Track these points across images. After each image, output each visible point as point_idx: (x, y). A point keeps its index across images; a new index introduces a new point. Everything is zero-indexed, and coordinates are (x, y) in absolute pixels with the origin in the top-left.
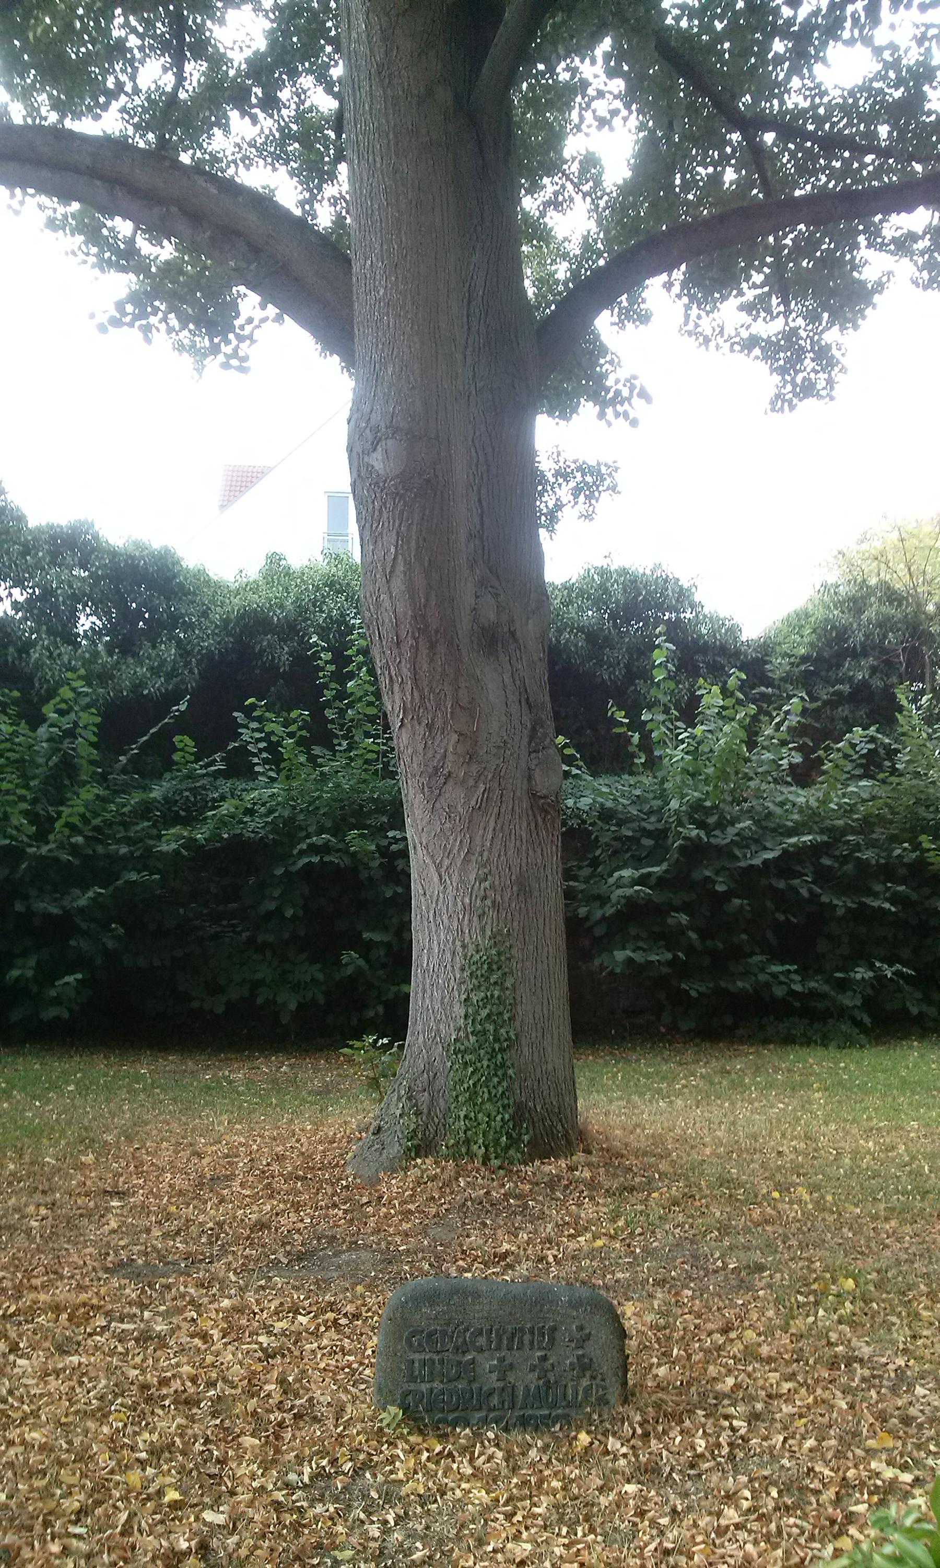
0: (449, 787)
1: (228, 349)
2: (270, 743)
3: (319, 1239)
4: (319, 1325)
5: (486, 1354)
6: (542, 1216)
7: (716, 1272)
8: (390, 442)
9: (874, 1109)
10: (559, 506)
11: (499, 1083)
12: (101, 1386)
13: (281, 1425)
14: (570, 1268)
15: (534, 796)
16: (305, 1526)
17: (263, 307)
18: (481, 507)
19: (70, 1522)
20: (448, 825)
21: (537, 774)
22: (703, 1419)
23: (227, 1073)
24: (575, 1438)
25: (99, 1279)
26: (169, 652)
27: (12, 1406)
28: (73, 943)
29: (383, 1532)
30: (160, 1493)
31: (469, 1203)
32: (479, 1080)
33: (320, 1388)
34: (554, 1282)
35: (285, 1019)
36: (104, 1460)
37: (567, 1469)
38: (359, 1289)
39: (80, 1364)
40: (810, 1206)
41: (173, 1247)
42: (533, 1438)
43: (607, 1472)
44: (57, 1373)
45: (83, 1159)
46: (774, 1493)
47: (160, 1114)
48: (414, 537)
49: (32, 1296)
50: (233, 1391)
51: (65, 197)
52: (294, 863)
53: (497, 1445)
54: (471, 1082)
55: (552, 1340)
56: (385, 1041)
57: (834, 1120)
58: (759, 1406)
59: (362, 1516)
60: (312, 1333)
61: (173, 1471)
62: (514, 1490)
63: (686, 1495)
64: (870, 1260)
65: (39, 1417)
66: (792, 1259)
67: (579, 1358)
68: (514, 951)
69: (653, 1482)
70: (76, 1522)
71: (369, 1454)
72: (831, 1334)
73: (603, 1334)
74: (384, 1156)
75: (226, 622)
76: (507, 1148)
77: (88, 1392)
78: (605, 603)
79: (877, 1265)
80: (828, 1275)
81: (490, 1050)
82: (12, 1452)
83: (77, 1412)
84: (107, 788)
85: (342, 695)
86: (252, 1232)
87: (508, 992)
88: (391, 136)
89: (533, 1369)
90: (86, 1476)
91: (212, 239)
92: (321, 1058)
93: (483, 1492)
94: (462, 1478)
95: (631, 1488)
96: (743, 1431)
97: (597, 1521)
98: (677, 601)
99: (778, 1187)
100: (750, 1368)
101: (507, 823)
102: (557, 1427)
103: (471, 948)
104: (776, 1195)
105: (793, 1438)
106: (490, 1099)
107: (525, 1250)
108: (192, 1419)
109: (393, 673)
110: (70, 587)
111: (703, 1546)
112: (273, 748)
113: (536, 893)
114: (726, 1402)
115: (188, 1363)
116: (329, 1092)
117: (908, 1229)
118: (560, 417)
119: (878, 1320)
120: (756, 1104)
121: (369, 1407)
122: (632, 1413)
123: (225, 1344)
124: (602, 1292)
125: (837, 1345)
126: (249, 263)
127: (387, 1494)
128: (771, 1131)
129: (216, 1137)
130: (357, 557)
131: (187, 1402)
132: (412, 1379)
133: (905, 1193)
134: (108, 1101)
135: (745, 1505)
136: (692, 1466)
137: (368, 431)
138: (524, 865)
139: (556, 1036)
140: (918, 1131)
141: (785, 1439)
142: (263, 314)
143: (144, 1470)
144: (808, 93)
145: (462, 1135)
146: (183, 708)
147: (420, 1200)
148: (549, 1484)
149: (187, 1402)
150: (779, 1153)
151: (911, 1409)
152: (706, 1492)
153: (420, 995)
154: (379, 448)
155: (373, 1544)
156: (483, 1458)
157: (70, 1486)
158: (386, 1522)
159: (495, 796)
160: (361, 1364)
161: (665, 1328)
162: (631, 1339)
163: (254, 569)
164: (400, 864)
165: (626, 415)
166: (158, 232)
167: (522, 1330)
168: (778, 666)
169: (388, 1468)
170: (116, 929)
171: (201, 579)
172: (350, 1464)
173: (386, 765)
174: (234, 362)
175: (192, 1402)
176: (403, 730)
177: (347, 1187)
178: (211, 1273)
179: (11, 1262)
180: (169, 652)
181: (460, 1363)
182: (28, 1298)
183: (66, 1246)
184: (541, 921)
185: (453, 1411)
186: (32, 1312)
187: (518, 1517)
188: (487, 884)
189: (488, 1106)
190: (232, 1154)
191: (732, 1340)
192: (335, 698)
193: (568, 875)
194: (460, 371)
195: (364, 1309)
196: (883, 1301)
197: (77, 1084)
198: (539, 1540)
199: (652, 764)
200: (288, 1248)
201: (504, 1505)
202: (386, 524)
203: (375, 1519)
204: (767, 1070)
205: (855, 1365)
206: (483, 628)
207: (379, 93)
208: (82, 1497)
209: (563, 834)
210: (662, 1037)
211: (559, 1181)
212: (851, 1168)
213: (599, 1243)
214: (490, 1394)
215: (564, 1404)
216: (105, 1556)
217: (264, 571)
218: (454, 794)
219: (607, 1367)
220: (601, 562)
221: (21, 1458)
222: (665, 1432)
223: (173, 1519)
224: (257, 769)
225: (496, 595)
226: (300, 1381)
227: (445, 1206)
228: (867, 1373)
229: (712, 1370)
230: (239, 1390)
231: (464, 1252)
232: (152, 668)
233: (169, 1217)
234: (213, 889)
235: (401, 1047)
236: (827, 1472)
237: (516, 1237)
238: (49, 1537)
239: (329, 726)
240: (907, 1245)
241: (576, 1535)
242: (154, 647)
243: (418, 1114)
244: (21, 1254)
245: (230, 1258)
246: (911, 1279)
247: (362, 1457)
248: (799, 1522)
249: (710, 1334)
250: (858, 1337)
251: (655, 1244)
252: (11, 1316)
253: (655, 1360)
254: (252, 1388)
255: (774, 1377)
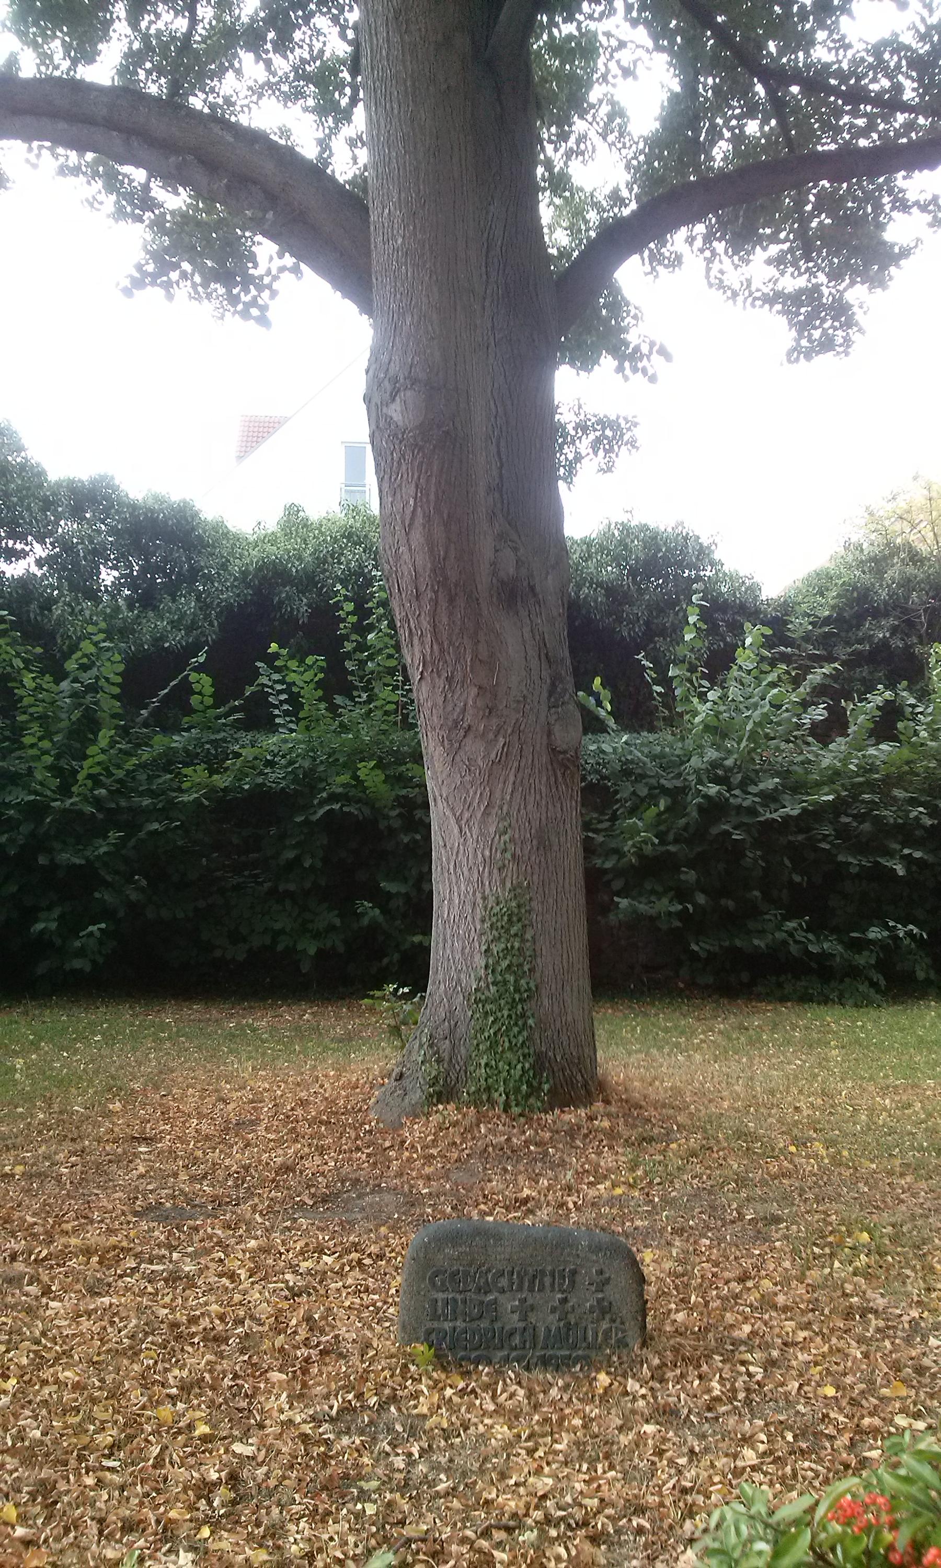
0: (468, 741)
1: (245, 298)
2: (291, 694)
3: (343, 1182)
4: (344, 1265)
5: (508, 1295)
6: (563, 1164)
7: (733, 1222)
8: (409, 393)
9: (891, 1068)
10: (578, 458)
11: (519, 1032)
12: (132, 1325)
13: (307, 1360)
14: (590, 1215)
15: (553, 751)
16: (331, 1457)
17: (281, 255)
18: (500, 459)
19: (103, 1455)
20: (468, 778)
21: (557, 729)
22: (720, 1365)
23: (250, 1021)
24: (595, 1379)
25: (129, 1223)
26: (188, 605)
27: (45, 1347)
28: (97, 895)
29: (408, 1464)
30: (191, 1427)
31: (491, 1149)
32: (500, 1029)
33: (345, 1325)
34: (575, 1227)
35: (305, 967)
36: (137, 1397)
37: (588, 1409)
38: (383, 1230)
39: (111, 1305)
40: (826, 1161)
41: (200, 1190)
42: (554, 1377)
43: (627, 1412)
44: (89, 1314)
45: (111, 1106)
46: (790, 1437)
47: (185, 1061)
48: (433, 489)
49: (63, 1240)
50: (261, 1329)
51: (81, 149)
52: (315, 812)
53: (519, 1383)
54: (492, 1031)
55: (573, 1283)
56: (406, 990)
57: (851, 1078)
58: (775, 1353)
59: (388, 1448)
60: (337, 1273)
61: (203, 1406)
62: (536, 1427)
63: (702, 1437)
64: (886, 1215)
65: (72, 1357)
66: (808, 1212)
67: (599, 1301)
68: (534, 904)
69: (672, 1424)
70: (108, 1457)
71: (395, 1390)
72: (846, 1285)
73: (621, 1280)
74: (406, 1101)
75: (244, 573)
76: (528, 1096)
77: (120, 1332)
78: (625, 560)
79: (892, 1220)
80: (843, 1229)
81: (510, 1000)
82: (46, 1390)
83: (109, 1351)
84: (129, 742)
85: (362, 647)
86: (277, 1175)
87: (528, 944)
88: (409, 84)
89: (554, 1310)
90: (119, 1412)
91: (228, 187)
92: (342, 1006)
93: (506, 1428)
94: (485, 1413)
95: (650, 1428)
96: (759, 1377)
97: (617, 1459)
98: (697, 558)
99: (795, 1141)
100: (766, 1317)
101: (527, 778)
102: (578, 1367)
103: (492, 900)
104: (793, 1149)
105: (808, 1385)
106: (510, 1048)
107: (545, 1196)
108: (221, 1355)
109: (413, 626)
110: (91, 542)
111: (720, 1486)
112: (294, 700)
113: (556, 848)
114: (743, 1348)
115: (217, 1302)
116: (350, 1039)
117: (923, 1185)
118: (581, 368)
119: (893, 1273)
120: (774, 1060)
121: (394, 1344)
122: (650, 1356)
123: (252, 1283)
124: (622, 1239)
125: (852, 1296)
126: (265, 211)
127: (411, 1427)
128: (788, 1087)
129: (241, 1081)
130: (375, 508)
131: (216, 1339)
132: (435, 1317)
133: (921, 1149)
134: (134, 1049)
135: (762, 1448)
136: (709, 1409)
137: (386, 382)
138: (543, 819)
139: (575, 989)
140: (934, 1089)
141: (801, 1385)
142: (281, 263)
143: (174, 1405)
144: (832, 45)
145: (483, 1082)
146: (202, 660)
147: (442, 1145)
148: (570, 1422)
149: (215, 1339)
150: (796, 1108)
151: (925, 1359)
152: (723, 1435)
153: (441, 945)
154: (397, 398)
155: (398, 1476)
156: (505, 1395)
157: (103, 1422)
158: (410, 1455)
159: (515, 751)
160: (385, 1303)
161: (683, 1275)
162: (650, 1285)
163: (272, 524)
164: (418, 814)
165: (644, 371)
166: (172, 180)
167: (543, 1272)
168: (799, 625)
169: (412, 1403)
170: (139, 880)
171: (220, 532)
172: (375, 1399)
173: (405, 717)
174: (255, 312)
175: (220, 1339)
176: (423, 683)
177: (370, 1132)
178: (238, 1215)
179: (42, 1210)
180: (188, 605)
181: (482, 1303)
182: (60, 1243)
183: (96, 1191)
184: (560, 874)
185: (476, 1349)
186: (63, 1256)
187: (540, 1453)
188: (507, 837)
189: (509, 1055)
190: (257, 1100)
191: (749, 1289)
192: (355, 650)
193: (587, 826)
194: (478, 322)
195: (388, 1250)
196: (898, 1254)
197: (103, 1035)
198: (560, 1476)
199: (673, 721)
200: (313, 1190)
201: (526, 1441)
202: (405, 476)
203: (400, 1451)
204: (784, 1027)
205: (870, 1316)
206: (503, 583)
207: (396, 39)
208: (114, 1432)
209: (583, 789)
210: (680, 993)
211: (579, 1129)
212: (868, 1125)
213: (618, 1191)
214: (511, 1334)
215: (584, 1345)
216: (139, 1487)
217: (282, 523)
218: (473, 747)
219: (627, 1310)
220: (623, 518)
221: (55, 1396)
222: (682, 1376)
223: (203, 1452)
224: (278, 721)
225: (515, 549)
226: (325, 1318)
227: (467, 1152)
228: (881, 1324)
229: (729, 1317)
230: (266, 1328)
231: (485, 1196)
232: (172, 622)
233: (195, 1162)
234: (235, 840)
235: (423, 998)
236: (841, 1419)
237: (537, 1183)
238: (83, 1471)
239: (349, 678)
240: (922, 1201)
241: (596, 1471)
242: (174, 601)
243: (439, 1061)
244: (52, 1201)
245: (256, 1200)
246: (926, 1233)
247: (387, 1391)
248: (813, 1466)
249: (727, 1282)
250: (873, 1289)
251: (673, 1194)
252: (43, 1260)
253: (673, 1306)
254: (279, 1327)
255: (790, 1325)
